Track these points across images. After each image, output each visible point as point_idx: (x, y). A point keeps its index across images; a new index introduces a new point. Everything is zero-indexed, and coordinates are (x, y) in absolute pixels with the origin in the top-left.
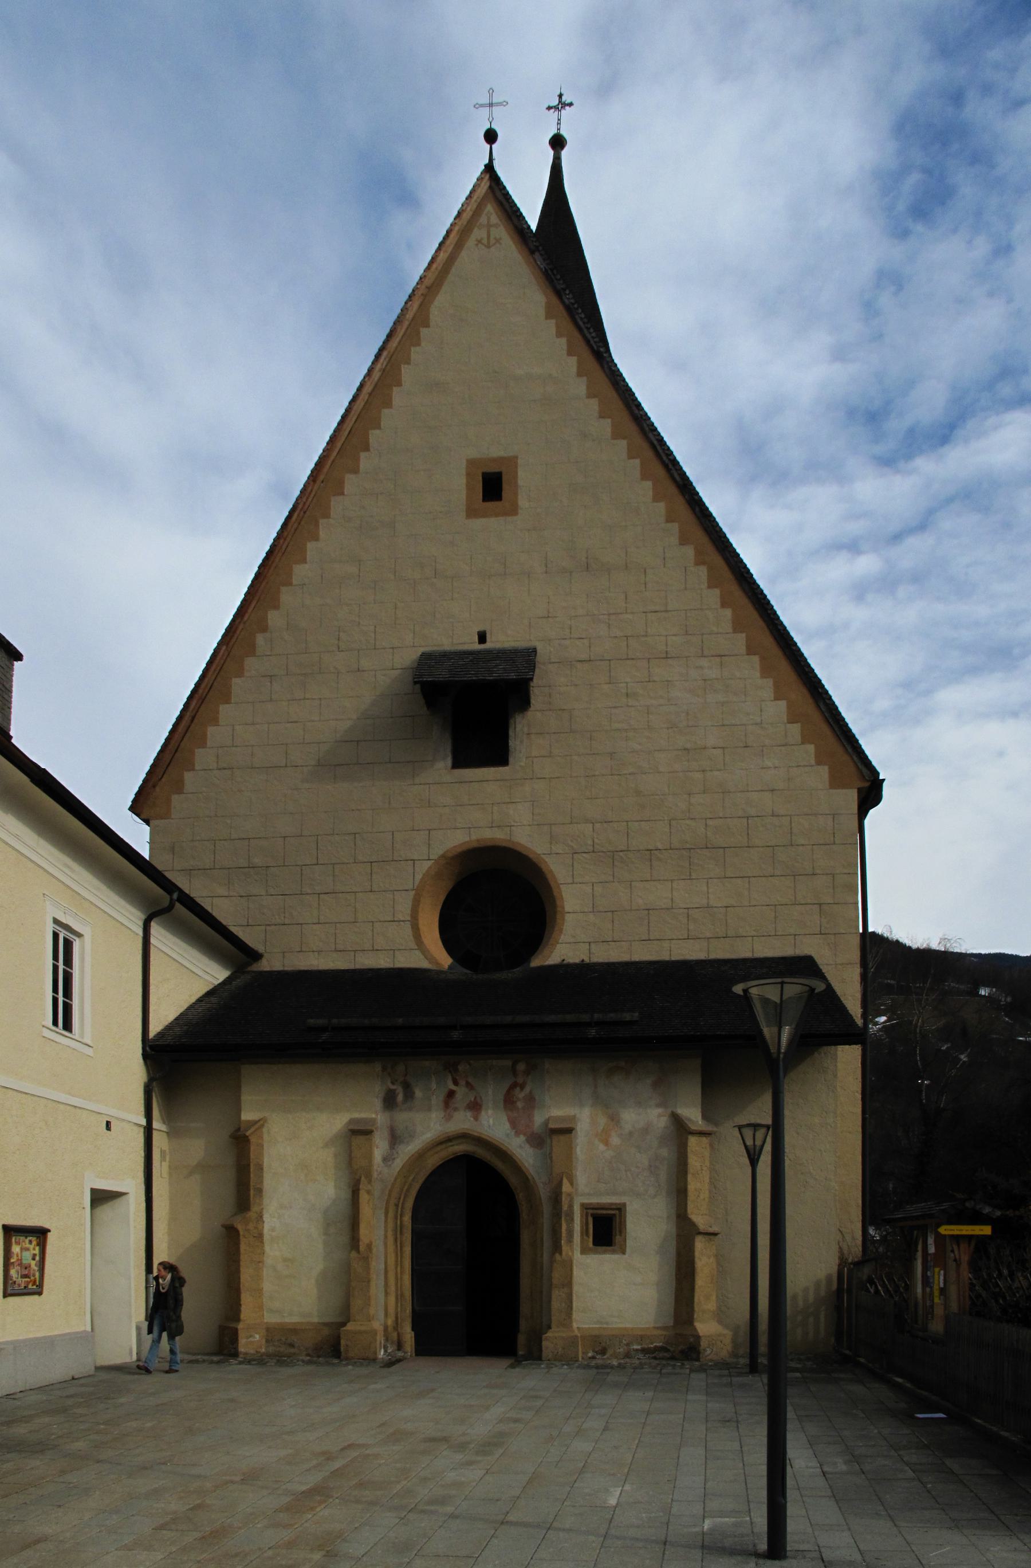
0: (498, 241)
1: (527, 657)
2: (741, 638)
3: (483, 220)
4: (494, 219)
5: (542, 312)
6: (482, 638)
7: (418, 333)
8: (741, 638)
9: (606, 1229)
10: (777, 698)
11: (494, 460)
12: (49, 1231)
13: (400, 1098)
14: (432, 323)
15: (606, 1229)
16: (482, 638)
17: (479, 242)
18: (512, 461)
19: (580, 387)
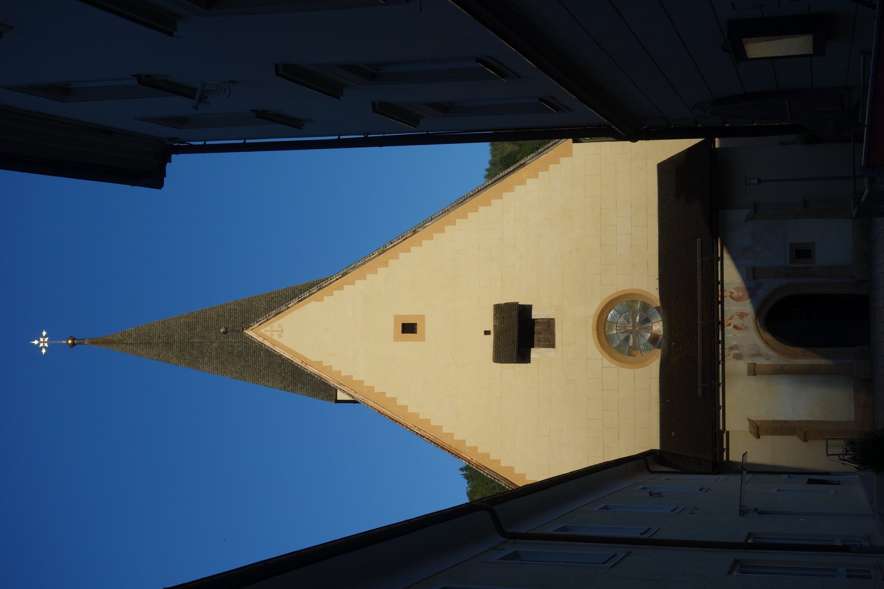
0: (280, 326)
1: (500, 310)
2: (494, 202)
3: (268, 334)
4: (268, 328)
5: (319, 303)
6: (487, 333)
7: (326, 367)
8: (494, 202)
9: (802, 253)
10: (525, 183)
11: (424, 331)
12: (749, 419)
13: (737, 352)
14: (320, 359)
15: (802, 253)
16: (487, 333)
17: (280, 336)
18: (396, 318)
19: (359, 283)
